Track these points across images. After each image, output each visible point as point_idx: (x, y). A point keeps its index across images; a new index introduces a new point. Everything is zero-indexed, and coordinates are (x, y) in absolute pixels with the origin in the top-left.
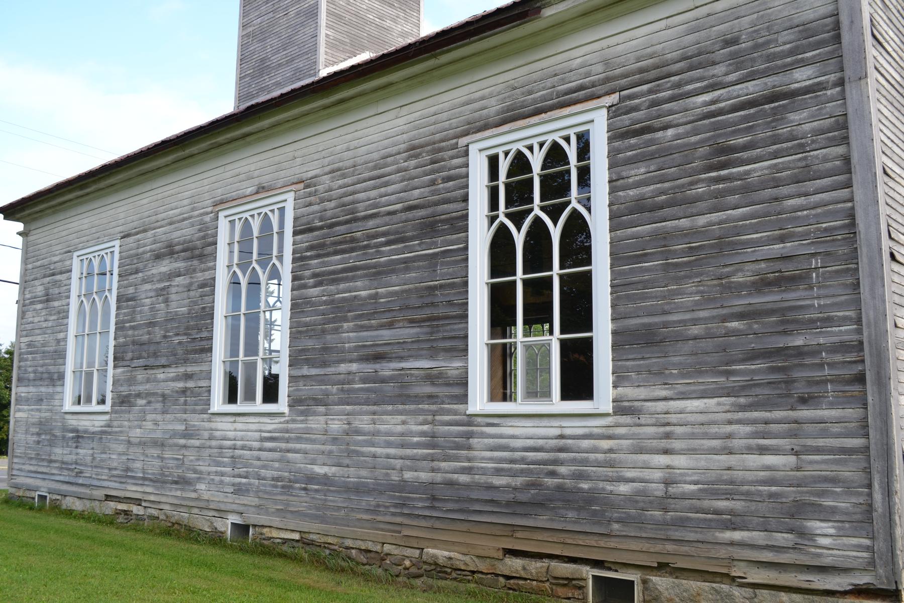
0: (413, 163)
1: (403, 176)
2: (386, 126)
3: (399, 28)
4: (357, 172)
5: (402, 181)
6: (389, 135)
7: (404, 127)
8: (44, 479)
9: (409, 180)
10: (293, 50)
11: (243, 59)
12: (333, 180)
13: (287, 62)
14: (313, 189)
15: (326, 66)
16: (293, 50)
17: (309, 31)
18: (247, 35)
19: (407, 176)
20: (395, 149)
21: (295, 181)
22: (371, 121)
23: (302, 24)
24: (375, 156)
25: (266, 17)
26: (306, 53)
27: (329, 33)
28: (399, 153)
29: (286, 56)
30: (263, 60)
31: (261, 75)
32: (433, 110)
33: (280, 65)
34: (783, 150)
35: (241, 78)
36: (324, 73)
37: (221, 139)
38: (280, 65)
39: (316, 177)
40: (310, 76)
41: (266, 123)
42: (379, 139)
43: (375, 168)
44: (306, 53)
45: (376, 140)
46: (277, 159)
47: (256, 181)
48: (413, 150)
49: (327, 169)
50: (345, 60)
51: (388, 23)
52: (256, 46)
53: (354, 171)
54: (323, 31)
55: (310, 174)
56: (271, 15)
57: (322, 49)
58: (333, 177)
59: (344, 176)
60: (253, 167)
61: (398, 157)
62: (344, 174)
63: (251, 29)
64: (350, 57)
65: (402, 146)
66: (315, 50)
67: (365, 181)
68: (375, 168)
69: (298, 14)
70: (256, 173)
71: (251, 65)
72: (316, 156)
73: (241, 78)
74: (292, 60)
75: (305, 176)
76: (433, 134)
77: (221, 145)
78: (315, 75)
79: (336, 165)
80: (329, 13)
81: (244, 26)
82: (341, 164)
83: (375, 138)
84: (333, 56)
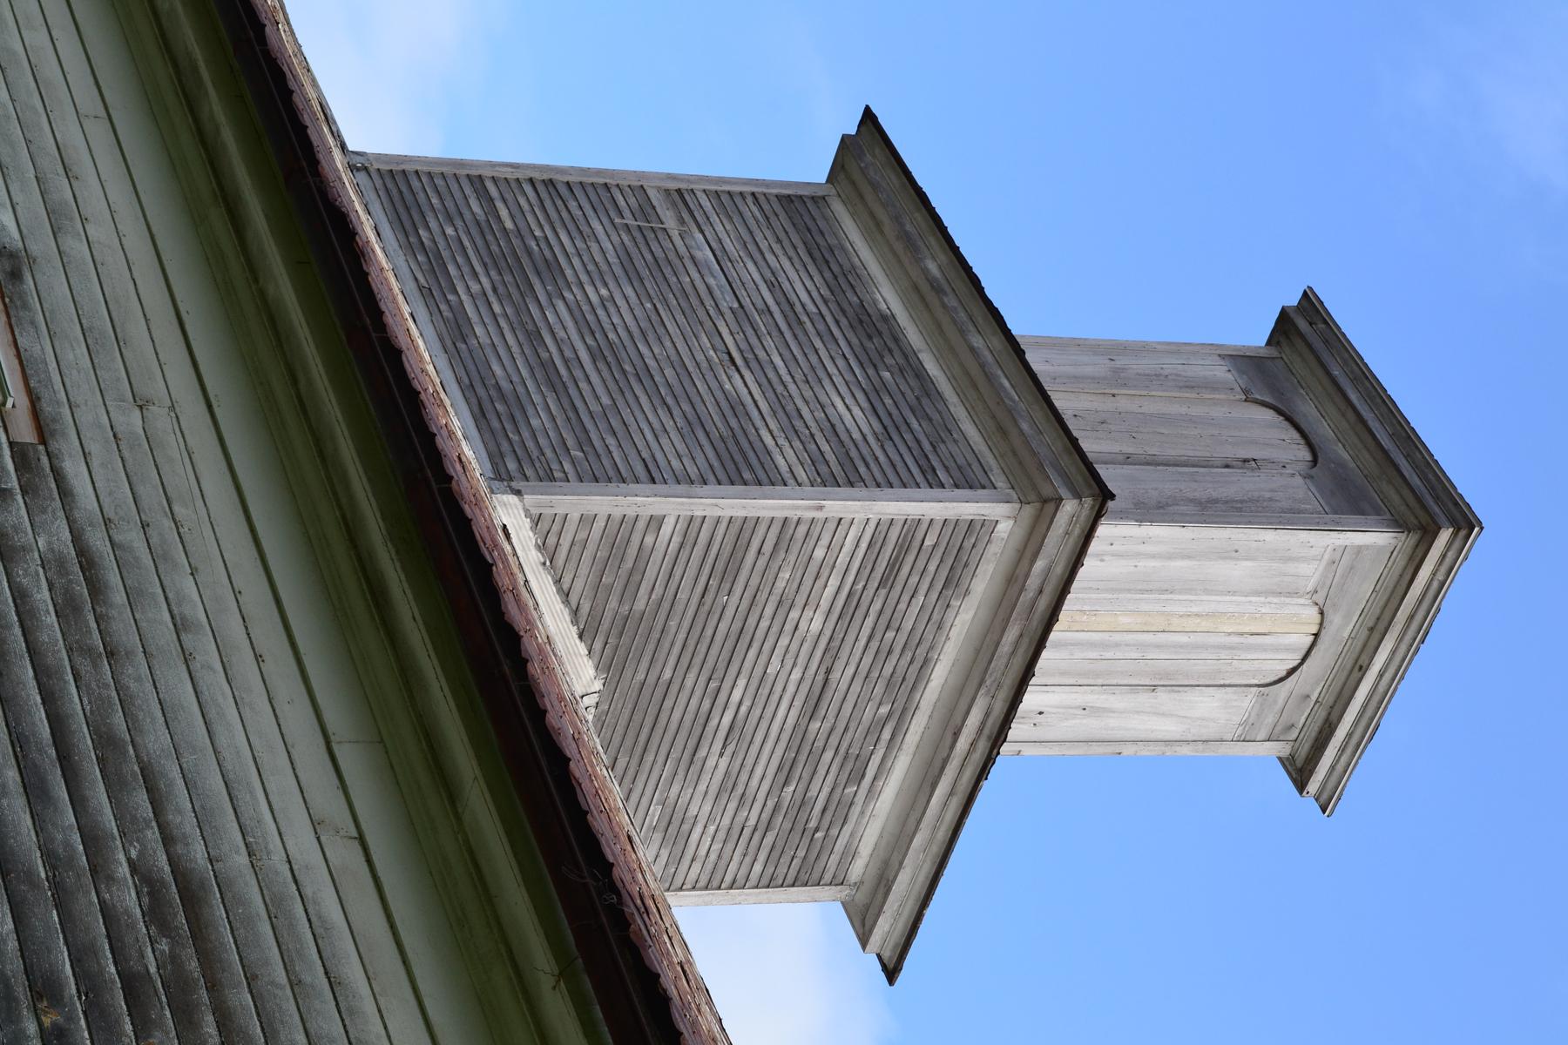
0: (129, 900)
1: (71, 860)
2: (281, 782)
3: (700, 807)
4: (85, 666)
5: (49, 856)
6: (243, 797)
7: (278, 857)
8: (975, 386)
9: (56, 885)
10: (595, 386)
11: (552, 189)
12: (52, 564)
13: (547, 366)
14: (13, 483)
15: (536, 521)
16: (595, 386)
17: (672, 450)
18: (646, 209)
19: (70, 879)
20: (184, 822)
21: (46, 408)
22: (298, 718)
23: (695, 424)
24: (156, 740)
25: (717, 281)
26: (584, 442)
27: (667, 529)
28: (168, 840)
29: (574, 362)
30: (551, 269)
31: (493, 262)
32: (353, 972)
33: (534, 337)
34: (920, 294)
35: (479, 182)
36: (511, 518)
37: (216, 107)
38: (534, 337)
39: (65, 493)
40: (495, 459)
41: (284, 288)
42: (226, 754)
43: (105, 742)
44: (584, 442)
45: (222, 741)
46: (136, 329)
47: (42, 245)
48: (182, 899)
49: (97, 540)
50: (565, 596)
51: (716, 764)
52: (606, 241)
53: (89, 651)
54: (671, 507)
55: (74, 468)
56: (727, 301)
57: (605, 504)
58: (61, 563)
59: (67, 610)
60: (100, 232)
61: (153, 834)
62: (77, 609)
63: (670, 222)
64: (575, 613)
65: (199, 852)
66: (599, 474)
67: (50, 699)
68: (105, 742)
69: (736, 406)
70: (77, 248)
71: (502, 221)
72: (150, 493)
73: (477, 182)
74: (553, 382)
75: (68, 447)
76: (251, 979)
77: (191, 103)
78: (502, 477)
79: (113, 578)
80: (744, 529)
81: (681, 195)
82: (119, 597)
83: (232, 737)
84: (578, 546)
